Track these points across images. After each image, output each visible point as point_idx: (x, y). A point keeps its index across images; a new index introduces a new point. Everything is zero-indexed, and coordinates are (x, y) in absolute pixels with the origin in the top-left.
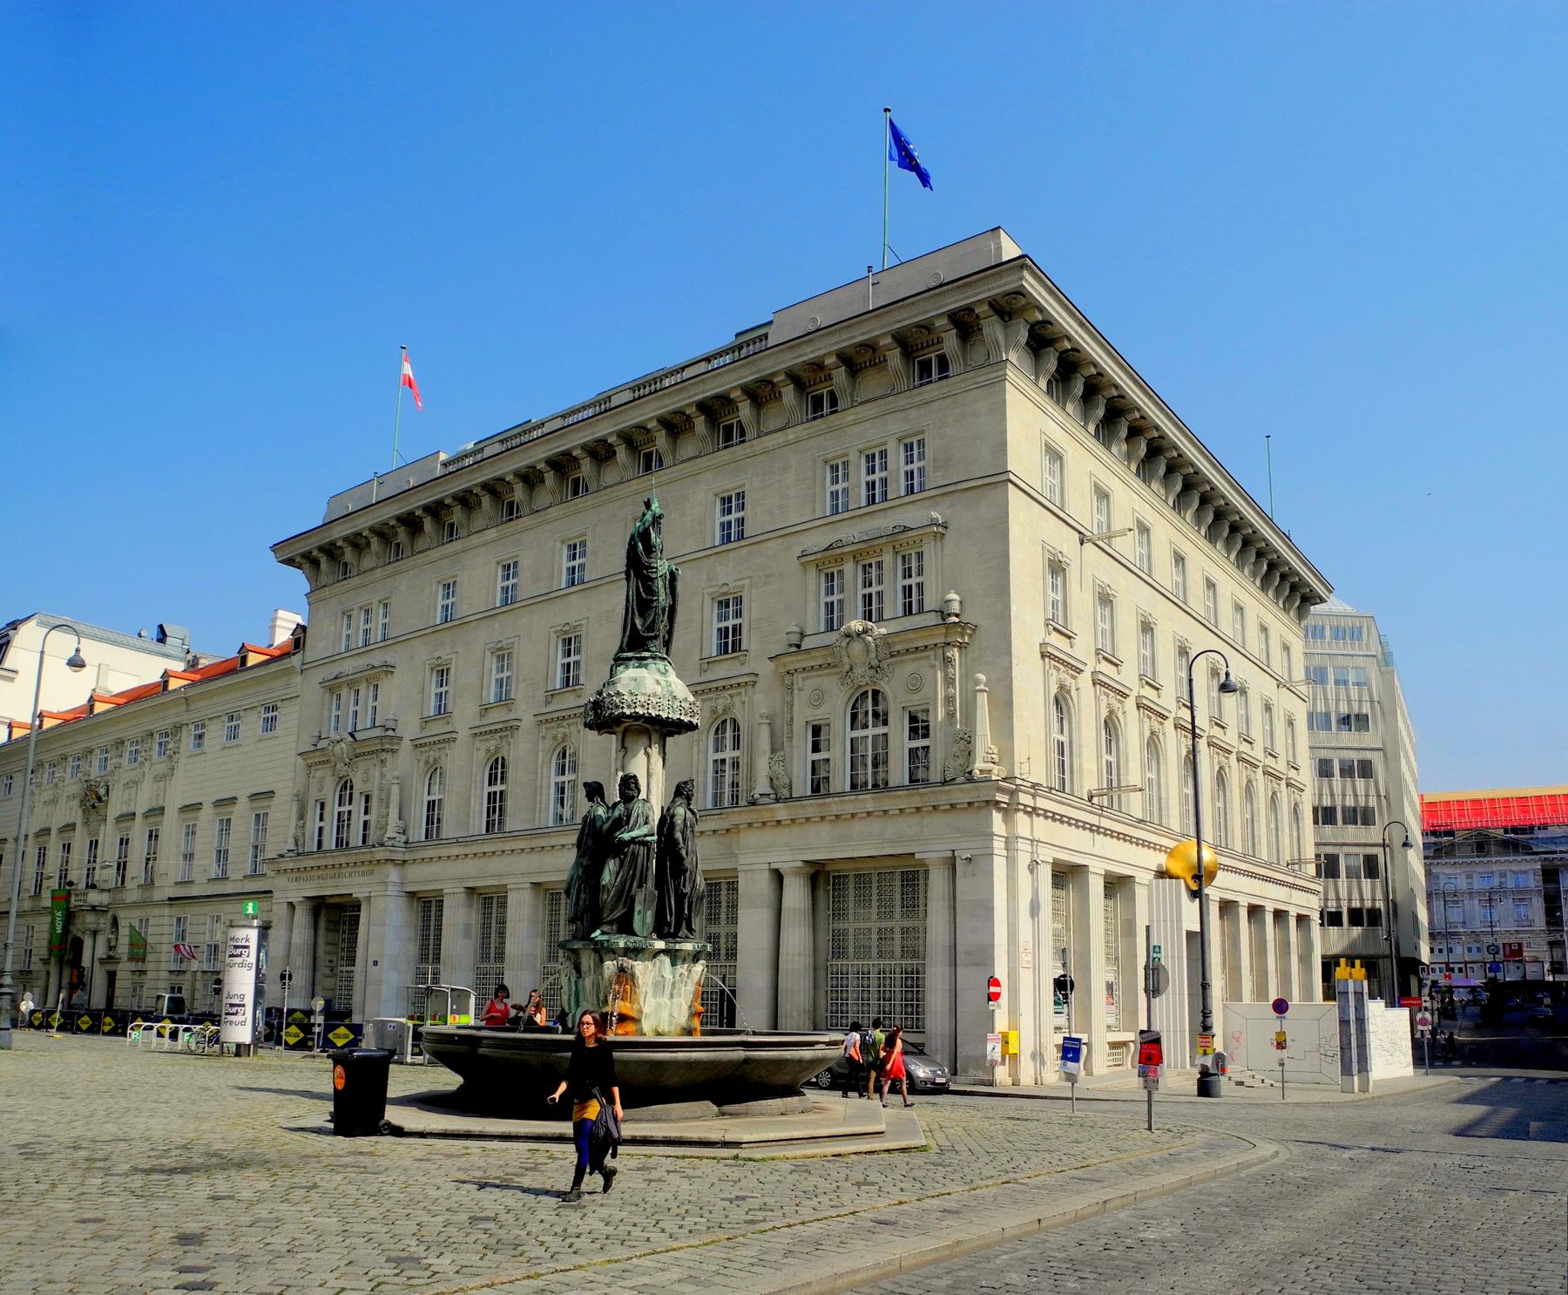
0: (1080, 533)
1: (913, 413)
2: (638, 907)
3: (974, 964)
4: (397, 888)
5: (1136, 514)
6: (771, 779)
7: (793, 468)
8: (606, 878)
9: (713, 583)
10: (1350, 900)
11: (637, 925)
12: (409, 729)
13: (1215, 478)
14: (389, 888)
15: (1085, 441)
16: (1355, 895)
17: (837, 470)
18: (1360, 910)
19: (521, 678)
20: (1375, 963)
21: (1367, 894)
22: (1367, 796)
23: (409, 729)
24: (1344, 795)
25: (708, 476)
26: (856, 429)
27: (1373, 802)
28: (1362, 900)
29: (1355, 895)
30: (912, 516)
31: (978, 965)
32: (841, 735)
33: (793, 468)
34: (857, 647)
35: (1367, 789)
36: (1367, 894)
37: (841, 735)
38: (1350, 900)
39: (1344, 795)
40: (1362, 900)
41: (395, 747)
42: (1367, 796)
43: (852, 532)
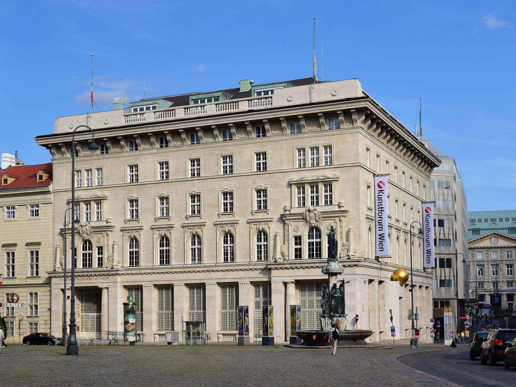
0: (373, 173)
1: (327, 138)
2: (339, 308)
3: (350, 311)
4: (120, 284)
5: (386, 159)
6: (281, 253)
7: (285, 149)
8: (333, 303)
9: (255, 184)
10: (441, 276)
11: (339, 312)
12: (118, 223)
13: (408, 139)
14: (118, 284)
15: (375, 141)
16: (443, 274)
17: (302, 150)
18: (444, 281)
19: (173, 209)
20: (449, 301)
21: (447, 274)
22: (449, 234)
23: (118, 223)
24: (440, 234)
25: (251, 145)
26: (308, 139)
27: (451, 237)
28: (445, 276)
29: (443, 274)
30: (329, 174)
31: (352, 311)
32: (306, 241)
33: (285, 149)
34: (312, 214)
35: (448, 192)
36: (447, 274)
37: (306, 241)
38: (441, 276)
39: (440, 234)
40: (445, 276)
41: (113, 230)
42: (449, 234)
43: (309, 176)
